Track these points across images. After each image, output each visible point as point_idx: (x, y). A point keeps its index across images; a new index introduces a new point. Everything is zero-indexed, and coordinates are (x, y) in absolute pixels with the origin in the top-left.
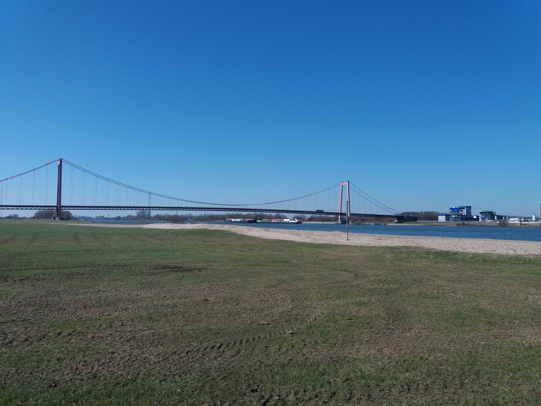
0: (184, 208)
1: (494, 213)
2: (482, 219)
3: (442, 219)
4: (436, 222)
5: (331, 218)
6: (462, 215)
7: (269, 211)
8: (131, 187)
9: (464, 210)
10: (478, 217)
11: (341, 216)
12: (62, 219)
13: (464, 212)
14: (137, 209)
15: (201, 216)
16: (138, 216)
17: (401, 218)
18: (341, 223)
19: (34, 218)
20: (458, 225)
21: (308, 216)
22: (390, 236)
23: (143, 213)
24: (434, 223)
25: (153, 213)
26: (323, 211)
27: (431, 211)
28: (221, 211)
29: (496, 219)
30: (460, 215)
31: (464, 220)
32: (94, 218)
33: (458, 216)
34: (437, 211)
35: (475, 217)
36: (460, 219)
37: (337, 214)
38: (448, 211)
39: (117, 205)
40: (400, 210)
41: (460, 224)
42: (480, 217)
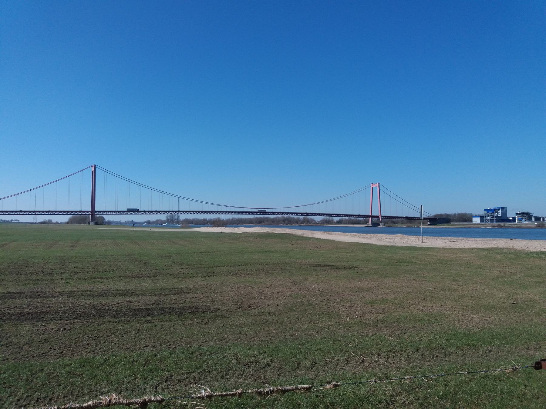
0: (205, 212)
1: (531, 214)
2: (519, 220)
3: (476, 220)
4: (514, 224)
5: (361, 221)
6: (497, 217)
7: (298, 215)
8: (162, 192)
9: (499, 211)
10: (514, 218)
11: (371, 219)
12: (96, 224)
13: (500, 213)
14: (166, 213)
15: (229, 219)
16: (168, 219)
17: (434, 220)
18: (371, 226)
19: (68, 223)
20: (493, 227)
21: (336, 219)
22: (457, 238)
23: (172, 217)
24: (468, 224)
25: (182, 217)
26: (18, 221)
27: (464, 213)
28: (245, 214)
29: (533, 220)
30: (496, 217)
31: (500, 222)
32: (123, 223)
33: (493, 217)
34: (471, 213)
35: (511, 219)
36: (495, 221)
37: (368, 216)
38: (482, 213)
39: (150, 210)
40: (431, 211)
41: (496, 225)
42: (516, 219)
